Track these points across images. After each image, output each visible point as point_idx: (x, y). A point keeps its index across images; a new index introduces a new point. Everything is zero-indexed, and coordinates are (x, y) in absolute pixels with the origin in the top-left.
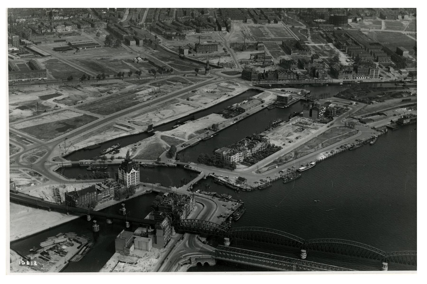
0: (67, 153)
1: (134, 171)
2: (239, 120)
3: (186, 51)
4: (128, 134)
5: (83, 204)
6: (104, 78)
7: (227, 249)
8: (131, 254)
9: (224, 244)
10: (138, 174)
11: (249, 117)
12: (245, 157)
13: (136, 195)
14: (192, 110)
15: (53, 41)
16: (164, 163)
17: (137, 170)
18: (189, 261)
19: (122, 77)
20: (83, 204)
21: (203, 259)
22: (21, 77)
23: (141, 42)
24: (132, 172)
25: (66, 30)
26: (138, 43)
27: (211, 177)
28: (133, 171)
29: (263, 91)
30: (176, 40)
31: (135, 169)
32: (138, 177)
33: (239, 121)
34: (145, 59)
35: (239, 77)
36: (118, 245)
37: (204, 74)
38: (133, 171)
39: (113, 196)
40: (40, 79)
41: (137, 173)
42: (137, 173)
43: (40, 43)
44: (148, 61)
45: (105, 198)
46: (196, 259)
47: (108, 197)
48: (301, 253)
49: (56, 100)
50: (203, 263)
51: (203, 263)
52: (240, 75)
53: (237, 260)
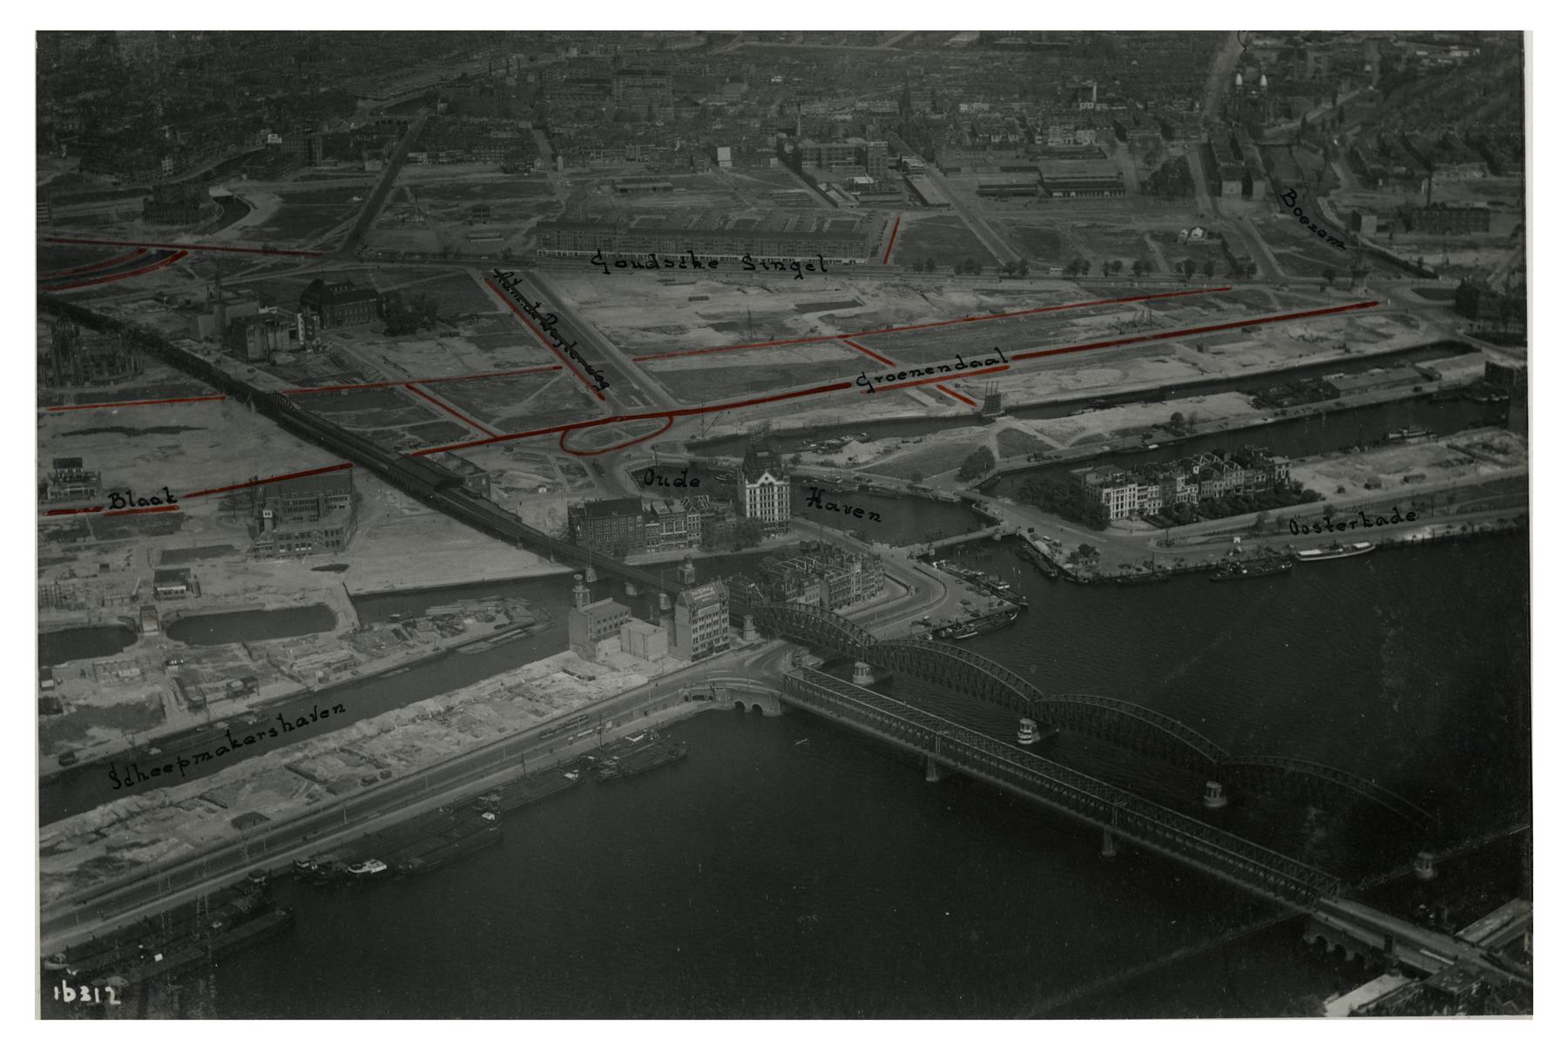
0: (708, 437)
1: (771, 479)
2: (1289, 416)
3: (1369, 223)
4: (922, 414)
5: (599, 541)
6: (1023, 274)
7: (857, 693)
8: (601, 657)
9: (851, 679)
10: (786, 491)
11: (1340, 413)
12: (1166, 503)
13: (760, 549)
14: (1192, 376)
15: (997, 169)
16: (925, 490)
17: (780, 479)
18: (709, 693)
19: (1080, 275)
20: (599, 541)
21: (748, 694)
22: (792, 252)
23: (1259, 187)
24: (762, 480)
25: (1076, 142)
26: (1247, 191)
27: (1022, 538)
28: (767, 478)
29: (1478, 351)
30: (1390, 189)
31: (774, 475)
32: (786, 497)
33: (1292, 421)
34: (1211, 235)
35: (1447, 308)
36: (576, 632)
37: (1349, 290)
38: (767, 478)
39: (696, 537)
40: (846, 261)
41: (780, 488)
42: (780, 488)
43: (958, 170)
44: (1217, 242)
45: (668, 538)
46: (732, 691)
47: (681, 536)
48: (1019, 726)
49: (831, 316)
50: (748, 706)
51: (748, 706)
52: (1451, 302)
53: (1143, 838)
